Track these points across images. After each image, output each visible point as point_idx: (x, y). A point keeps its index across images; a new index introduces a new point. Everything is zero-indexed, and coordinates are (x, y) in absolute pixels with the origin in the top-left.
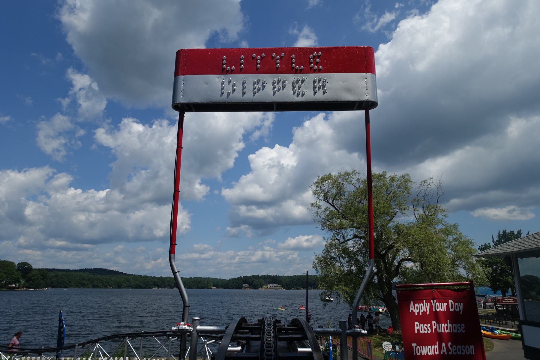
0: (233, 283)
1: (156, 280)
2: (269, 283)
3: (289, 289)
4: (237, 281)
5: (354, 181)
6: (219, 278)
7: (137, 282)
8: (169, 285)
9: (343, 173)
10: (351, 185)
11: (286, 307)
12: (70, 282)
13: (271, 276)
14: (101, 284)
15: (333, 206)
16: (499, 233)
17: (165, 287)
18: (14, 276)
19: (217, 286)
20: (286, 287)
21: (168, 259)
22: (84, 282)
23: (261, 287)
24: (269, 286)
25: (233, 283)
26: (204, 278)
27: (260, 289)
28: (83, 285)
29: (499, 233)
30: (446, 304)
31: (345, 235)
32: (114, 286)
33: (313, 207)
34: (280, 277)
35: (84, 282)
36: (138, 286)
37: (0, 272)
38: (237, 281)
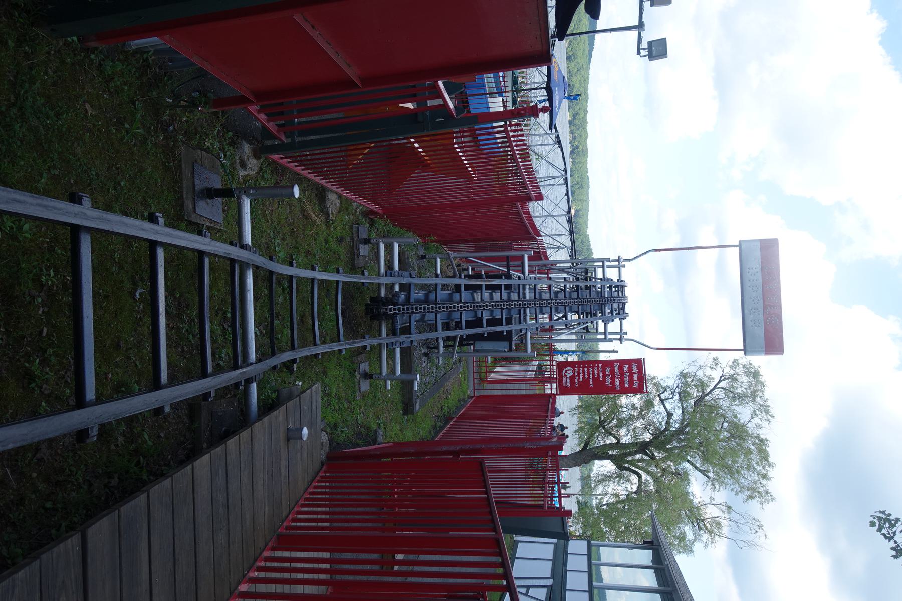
0: (582, 242)
1: (581, 116)
4: (586, 248)
5: (756, 420)
6: (589, 217)
8: (574, 138)
9: (768, 403)
10: (749, 416)
11: (547, 216)
15: (715, 388)
16: (893, 556)
17: (572, 132)
25: (582, 242)
26: (588, 194)
29: (893, 556)
30: (581, 380)
31: (671, 401)
32: (569, 49)
33: (711, 360)
38: (586, 248)
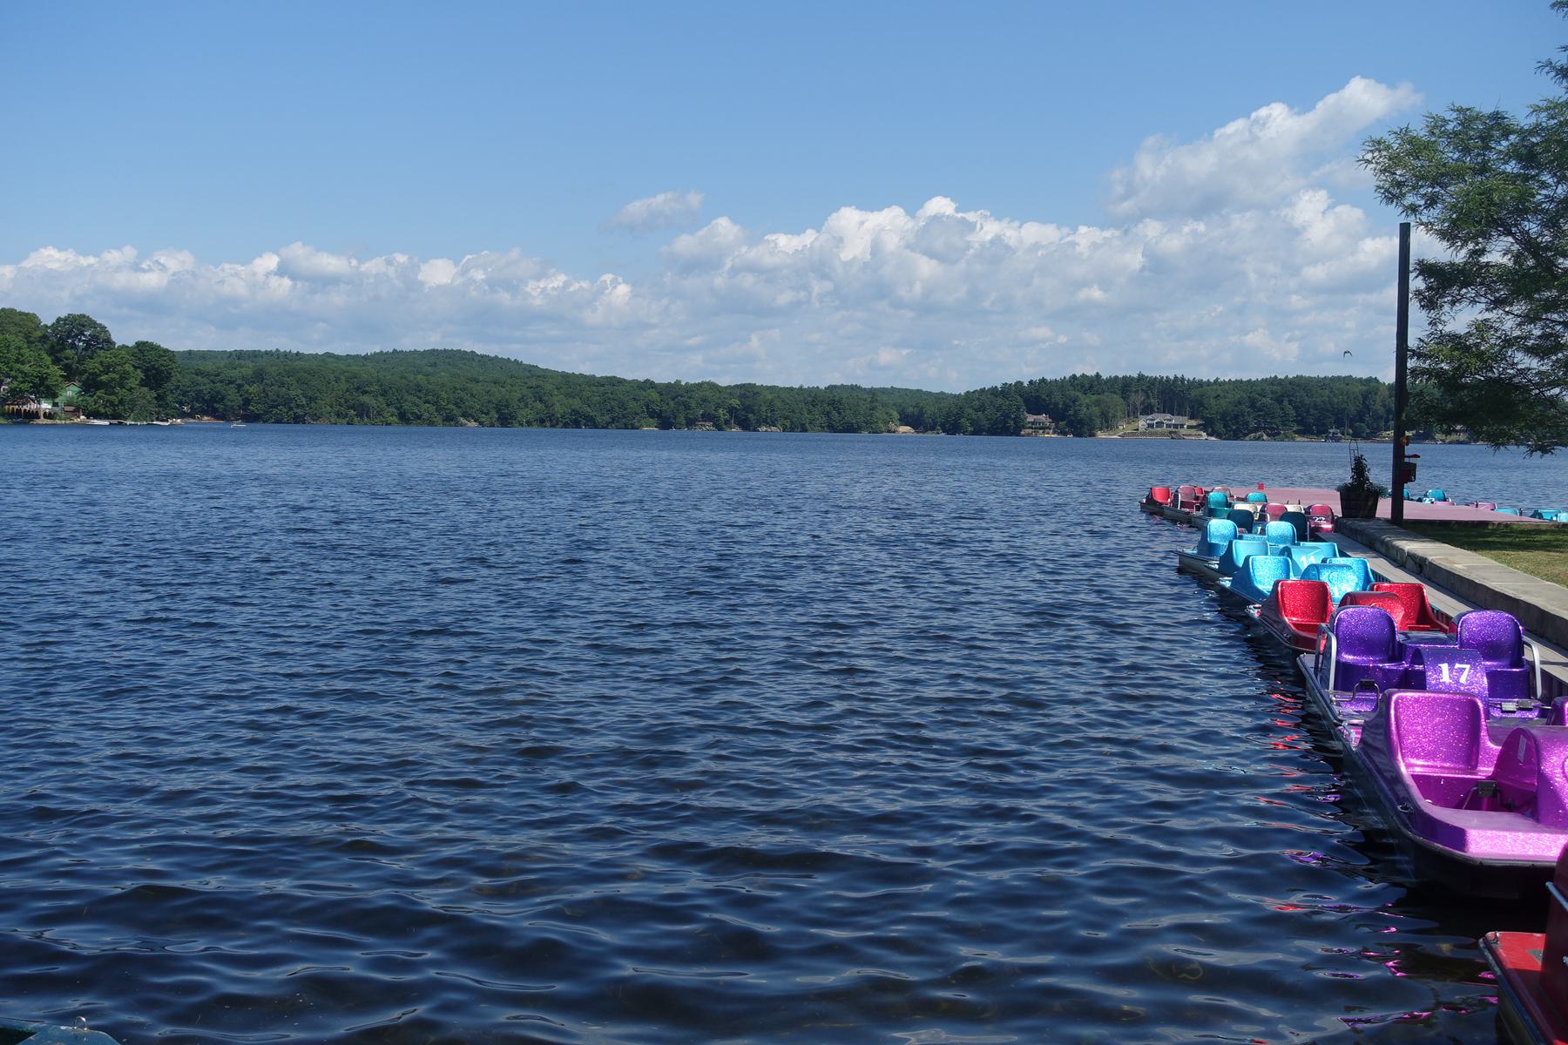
1: (654, 396)
2: (1148, 410)
3: (1236, 436)
6: (1313, 375)
7: (576, 403)
8: (707, 417)
12: (311, 399)
13: (1153, 382)
14: (432, 409)
18: (26, 368)
19: (917, 421)
20: (1220, 427)
21: (1397, 241)
22: (366, 399)
23: (1108, 424)
24: (1142, 423)
25: (982, 408)
27: (1101, 435)
28: (363, 412)
32: (483, 418)
34: (1201, 384)
35: (366, 399)
36: (576, 421)
37: (1567, 207)
